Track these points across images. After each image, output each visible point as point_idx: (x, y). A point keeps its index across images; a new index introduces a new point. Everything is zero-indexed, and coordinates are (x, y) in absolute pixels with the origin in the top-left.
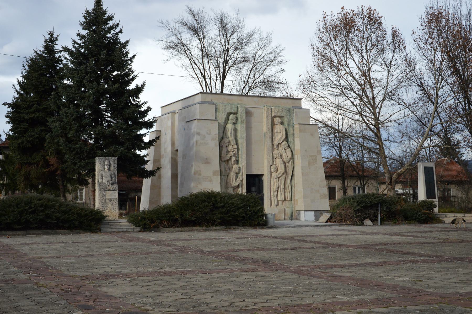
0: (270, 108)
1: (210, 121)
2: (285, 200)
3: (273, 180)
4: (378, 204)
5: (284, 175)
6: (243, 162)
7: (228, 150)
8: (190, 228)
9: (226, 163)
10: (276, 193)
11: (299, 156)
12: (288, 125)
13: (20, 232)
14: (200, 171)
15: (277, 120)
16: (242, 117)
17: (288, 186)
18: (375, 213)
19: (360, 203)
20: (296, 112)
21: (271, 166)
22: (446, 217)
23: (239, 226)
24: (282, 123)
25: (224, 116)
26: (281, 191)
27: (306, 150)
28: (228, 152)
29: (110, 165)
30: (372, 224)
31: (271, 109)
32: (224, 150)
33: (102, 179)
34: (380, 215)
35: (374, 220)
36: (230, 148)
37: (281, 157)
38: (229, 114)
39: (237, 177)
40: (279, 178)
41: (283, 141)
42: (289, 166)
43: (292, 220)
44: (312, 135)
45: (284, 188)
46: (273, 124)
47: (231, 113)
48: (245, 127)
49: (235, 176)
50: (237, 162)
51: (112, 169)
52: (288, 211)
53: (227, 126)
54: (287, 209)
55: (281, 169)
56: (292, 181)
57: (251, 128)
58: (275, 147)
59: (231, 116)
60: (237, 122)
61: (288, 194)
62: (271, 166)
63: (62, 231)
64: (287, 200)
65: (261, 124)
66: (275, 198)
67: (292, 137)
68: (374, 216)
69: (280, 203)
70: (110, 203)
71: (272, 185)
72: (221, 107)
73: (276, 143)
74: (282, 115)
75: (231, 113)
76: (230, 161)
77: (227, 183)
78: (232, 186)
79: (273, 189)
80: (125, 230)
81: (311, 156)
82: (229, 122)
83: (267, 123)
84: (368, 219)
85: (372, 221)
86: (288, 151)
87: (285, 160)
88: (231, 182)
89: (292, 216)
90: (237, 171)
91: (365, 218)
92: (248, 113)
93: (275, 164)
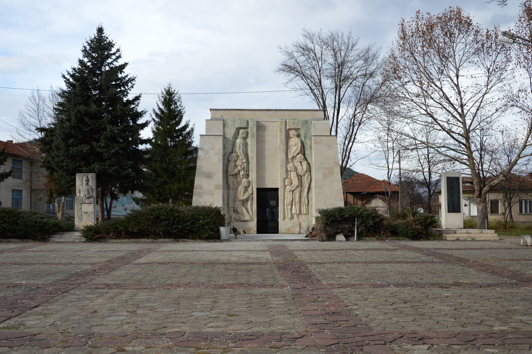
0: (284, 121)
2: (300, 213)
5: (299, 189)
6: (253, 176)
8: (137, 240)
9: (235, 177)
10: (290, 207)
12: (305, 137)
13: (14, 240)
14: (202, 185)
15: (292, 133)
16: (253, 131)
17: (304, 200)
22: (455, 233)
23: (188, 238)
24: (298, 136)
25: (233, 131)
27: (321, 163)
28: (236, 166)
29: (88, 180)
31: (286, 122)
32: (232, 165)
33: (80, 193)
34: (358, 229)
36: (239, 163)
38: (238, 129)
41: (298, 154)
42: (306, 180)
44: (328, 146)
45: (300, 201)
46: (288, 137)
47: (242, 128)
48: (255, 141)
49: (243, 190)
50: (247, 176)
51: (90, 184)
55: (296, 182)
56: (309, 194)
57: (265, 142)
59: (241, 131)
60: (247, 136)
61: (305, 207)
63: (14, 240)
65: (274, 139)
66: (289, 211)
68: (349, 231)
69: (295, 216)
70: (86, 216)
72: (229, 123)
73: (290, 156)
74: (298, 127)
75: (242, 128)
76: (238, 175)
80: (72, 240)
81: (327, 169)
83: (281, 136)
84: (342, 234)
86: (305, 164)
87: (300, 173)
88: (239, 196)
90: (246, 185)
91: (338, 233)
92: (260, 127)
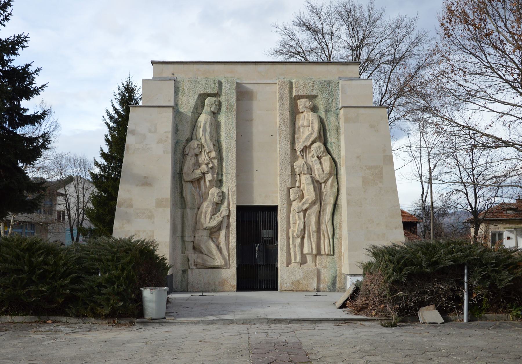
1: (157, 109)
2: (319, 253)
3: (293, 216)
4: (464, 264)
5: (316, 207)
6: (230, 183)
7: (197, 161)
10: (299, 240)
11: (344, 168)
12: (327, 112)
15: (302, 103)
17: (326, 227)
18: (452, 290)
19: (405, 265)
20: (342, 85)
21: (289, 189)
23: (97, 316)
24: (314, 109)
26: (309, 237)
27: (358, 157)
30: (440, 319)
32: (190, 161)
35: (448, 310)
36: (203, 158)
37: (310, 170)
38: (203, 97)
39: (214, 213)
40: (305, 211)
41: (313, 143)
42: (328, 190)
43: (334, 291)
44: (372, 126)
46: (294, 112)
50: (219, 183)
52: (326, 275)
53: (199, 119)
54: (323, 271)
55: (310, 194)
58: (298, 153)
59: (208, 101)
60: (219, 109)
61: (327, 241)
62: (289, 189)
64: (323, 252)
66: (298, 249)
67: (334, 133)
68: (450, 299)
69: (309, 258)
71: (291, 225)
72: (186, 86)
73: (299, 146)
74: (314, 93)
76: (202, 182)
77: (196, 222)
78: (205, 226)
79: (293, 232)
81: (370, 168)
82: (204, 111)
83: (282, 109)
84: (432, 307)
85: (444, 312)
86: (326, 160)
87: (317, 178)
89: (334, 283)
91: (423, 304)
92: (243, 95)
93: (297, 185)
